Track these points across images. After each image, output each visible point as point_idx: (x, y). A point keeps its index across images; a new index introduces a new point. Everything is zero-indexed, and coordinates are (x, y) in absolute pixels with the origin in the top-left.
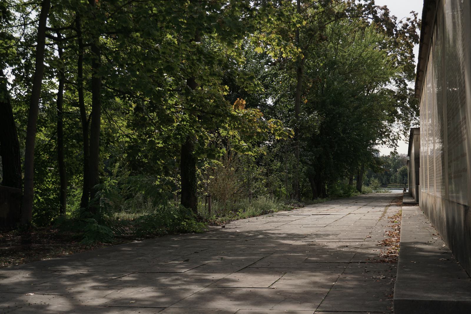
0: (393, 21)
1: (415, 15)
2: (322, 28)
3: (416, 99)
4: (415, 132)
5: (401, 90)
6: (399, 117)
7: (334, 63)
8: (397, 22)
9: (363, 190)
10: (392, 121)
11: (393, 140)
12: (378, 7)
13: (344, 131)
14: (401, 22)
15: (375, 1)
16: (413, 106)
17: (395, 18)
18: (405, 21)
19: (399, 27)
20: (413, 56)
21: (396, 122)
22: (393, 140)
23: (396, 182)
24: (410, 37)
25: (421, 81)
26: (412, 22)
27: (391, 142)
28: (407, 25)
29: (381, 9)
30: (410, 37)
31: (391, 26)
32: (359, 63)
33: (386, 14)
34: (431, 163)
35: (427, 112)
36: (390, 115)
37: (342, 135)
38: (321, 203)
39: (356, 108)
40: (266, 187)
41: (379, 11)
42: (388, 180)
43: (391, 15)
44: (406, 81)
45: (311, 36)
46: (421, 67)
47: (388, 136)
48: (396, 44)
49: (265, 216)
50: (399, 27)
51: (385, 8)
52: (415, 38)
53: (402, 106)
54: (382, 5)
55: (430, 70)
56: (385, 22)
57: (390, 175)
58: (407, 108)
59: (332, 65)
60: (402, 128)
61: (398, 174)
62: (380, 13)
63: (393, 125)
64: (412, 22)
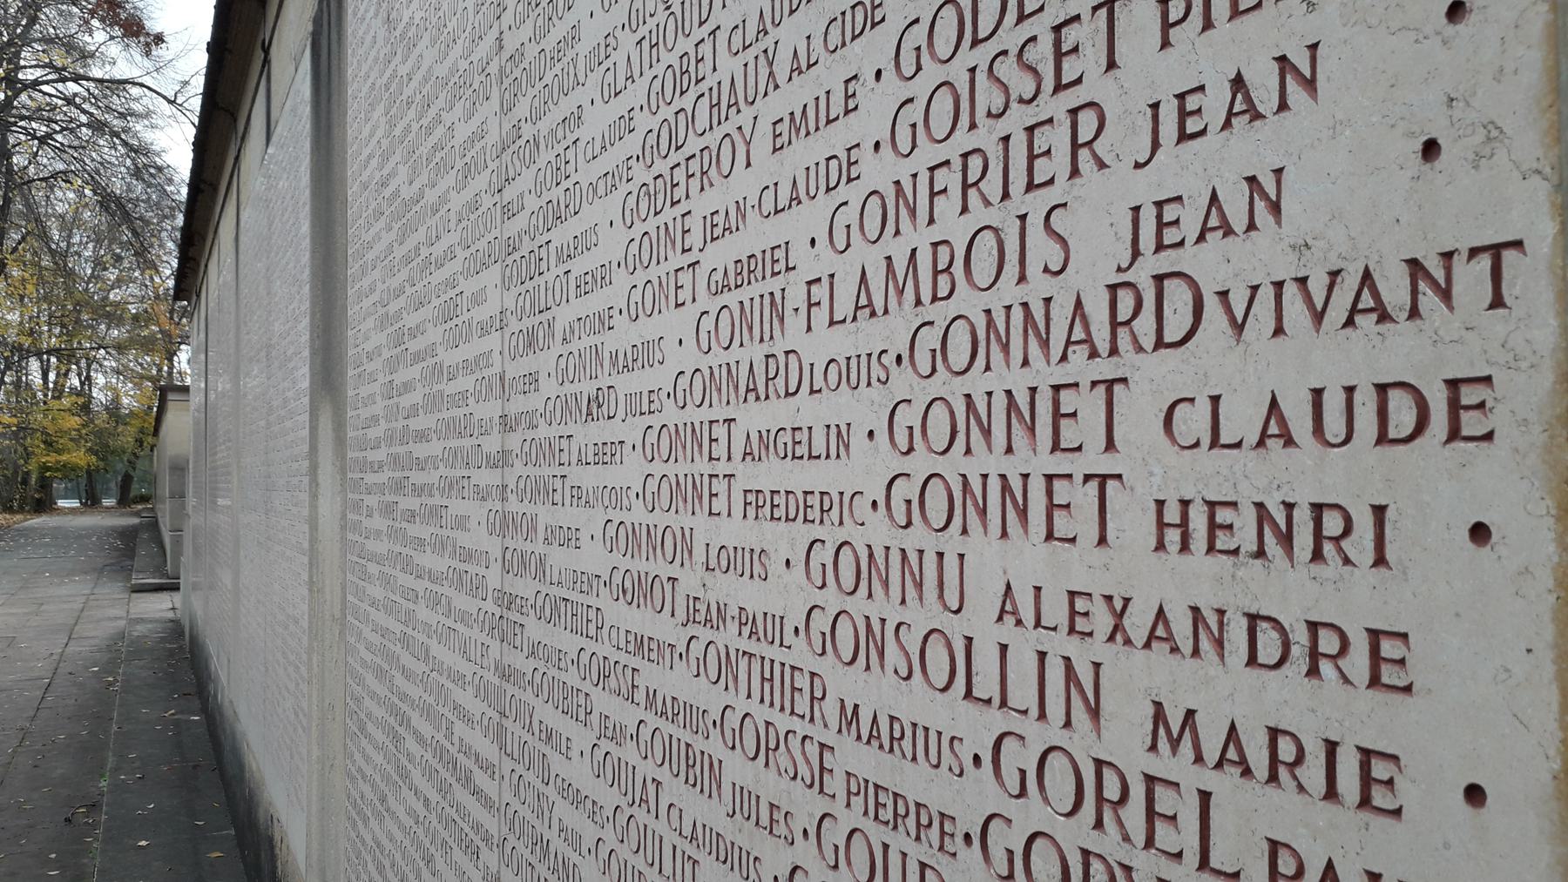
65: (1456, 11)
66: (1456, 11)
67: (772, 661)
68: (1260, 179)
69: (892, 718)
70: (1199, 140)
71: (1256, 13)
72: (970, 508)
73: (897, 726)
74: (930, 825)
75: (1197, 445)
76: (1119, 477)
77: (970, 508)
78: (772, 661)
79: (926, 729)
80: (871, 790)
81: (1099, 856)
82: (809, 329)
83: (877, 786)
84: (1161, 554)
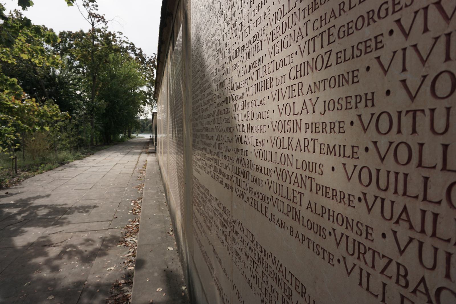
0: (144, 56)
1: (155, 55)
2: (107, 55)
3: (156, 94)
4: (155, 114)
5: (149, 91)
6: (148, 103)
7: (115, 75)
8: (146, 57)
9: (131, 136)
10: (144, 105)
11: (145, 114)
12: (137, 48)
13: (120, 111)
14: (148, 58)
15: (53, 12)
16: (154, 99)
17: (145, 55)
18: (150, 58)
19: (147, 60)
20: (153, 76)
21: (147, 106)
22: (145, 114)
23: (147, 130)
24: (153, 66)
25: (158, 89)
26: (154, 58)
27: (144, 115)
28: (151, 60)
29: (138, 49)
30: (153, 66)
31: (143, 59)
32: (128, 77)
33: (141, 52)
34: (161, 132)
35: (163, 102)
36: (144, 102)
37: (118, 112)
38: (102, 149)
39: (127, 99)
40: (69, 144)
41: (137, 50)
42: (144, 129)
43: (143, 53)
44: (151, 87)
45: (100, 60)
46: (158, 80)
47: (143, 112)
48: (146, 69)
49: (52, 171)
50: (147, 60)
51: (140, 49)
52: (154, 65)
53: (149, 98)
54: (139, 48)
55: (165, 83)
56: (140, 55)
57: (145, 128)
58: (152, 100)
59: (113, 77)
60: (149, 109)
61: (148, 127)
62: (138, 52)
63: (145, 107)
64: (154, 58)
65: (297, 303)
66: (297, 303)
67: (279, 184)
68: (344, 74)
69: (302, 235)
70: (345, 249)
71: (333, 43)
72: (298, 128)
73: (303, 237)
74: (336, 195)
75: (324, 154)
76: (344, 122)
77: (298, 128)
78: (279, 184)
79: (320, 227)
80: (324, 188)
81: (404, 266)
82: (279, 100)
83: (326, 187)
84: (400, 135)
